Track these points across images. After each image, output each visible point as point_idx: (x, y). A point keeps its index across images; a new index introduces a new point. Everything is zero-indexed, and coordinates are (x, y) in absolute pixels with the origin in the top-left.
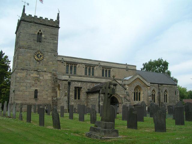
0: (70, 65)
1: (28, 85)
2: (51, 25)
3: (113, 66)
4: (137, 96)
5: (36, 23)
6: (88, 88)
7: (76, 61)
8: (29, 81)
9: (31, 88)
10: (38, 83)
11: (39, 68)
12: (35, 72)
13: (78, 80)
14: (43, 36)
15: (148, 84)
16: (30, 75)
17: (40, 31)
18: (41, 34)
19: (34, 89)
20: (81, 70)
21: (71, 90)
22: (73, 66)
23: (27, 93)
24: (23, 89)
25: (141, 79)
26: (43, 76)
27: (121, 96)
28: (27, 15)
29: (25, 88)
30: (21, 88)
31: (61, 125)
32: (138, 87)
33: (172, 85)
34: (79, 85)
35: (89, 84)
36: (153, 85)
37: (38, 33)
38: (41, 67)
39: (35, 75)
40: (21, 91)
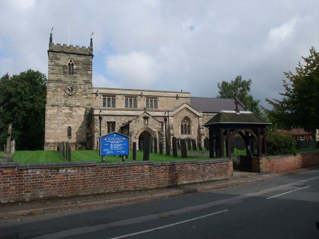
0: (111, 98)
1: (60, 122)
2: (82, 53)
3: (117, 93)
4: (186, 129)
5: (65, 53)
6: (123, 122)
7: (114, 92)
8: (61, 118)
9: (64, 125)
10: (71, 119)
11: (72, 103)
12: (67, 108)
13: (111, 114)
14: (75, 67)
15: (200, 114)
16: (61, 111)
17: (71, 61)
18: (73, 65)
19: (67, 126)
20: (120, 102)
21: (102, 125)
22: (111, 98)
23: (59, 131)
24: (55, 127)
25: (190, 108)
26: (76, 112)
27: (154, 130)
28: (55, 44)
29: (56, 125)
30: (53, 126)
31: (137, 157)
32: (187, 118)
33: (209, 113)
34: (112, 119)
35: (123, 118)
36: (206, 114)
37: (69, 64)
38: (72, 101)
39: (67, 110)
40: (53, 129)
